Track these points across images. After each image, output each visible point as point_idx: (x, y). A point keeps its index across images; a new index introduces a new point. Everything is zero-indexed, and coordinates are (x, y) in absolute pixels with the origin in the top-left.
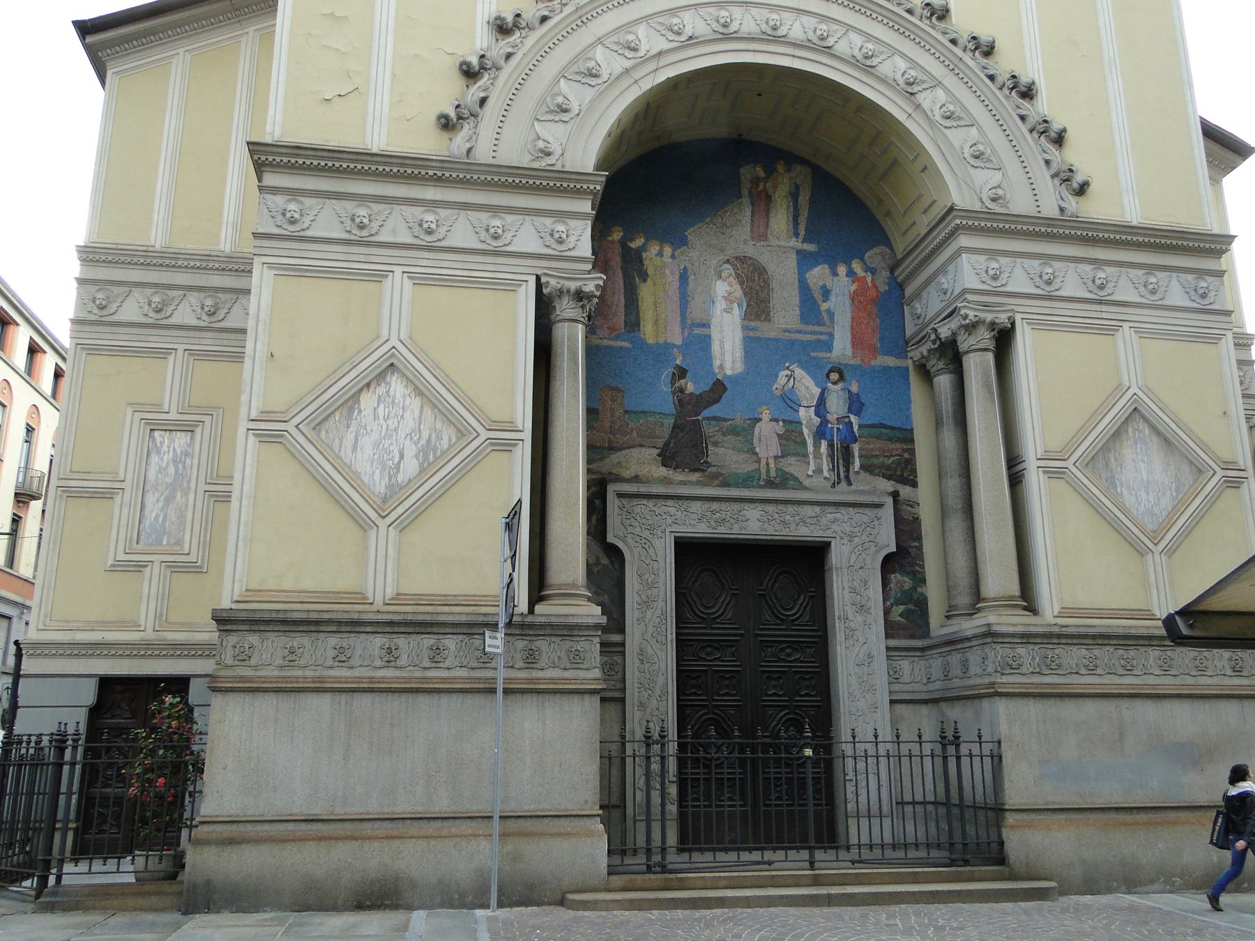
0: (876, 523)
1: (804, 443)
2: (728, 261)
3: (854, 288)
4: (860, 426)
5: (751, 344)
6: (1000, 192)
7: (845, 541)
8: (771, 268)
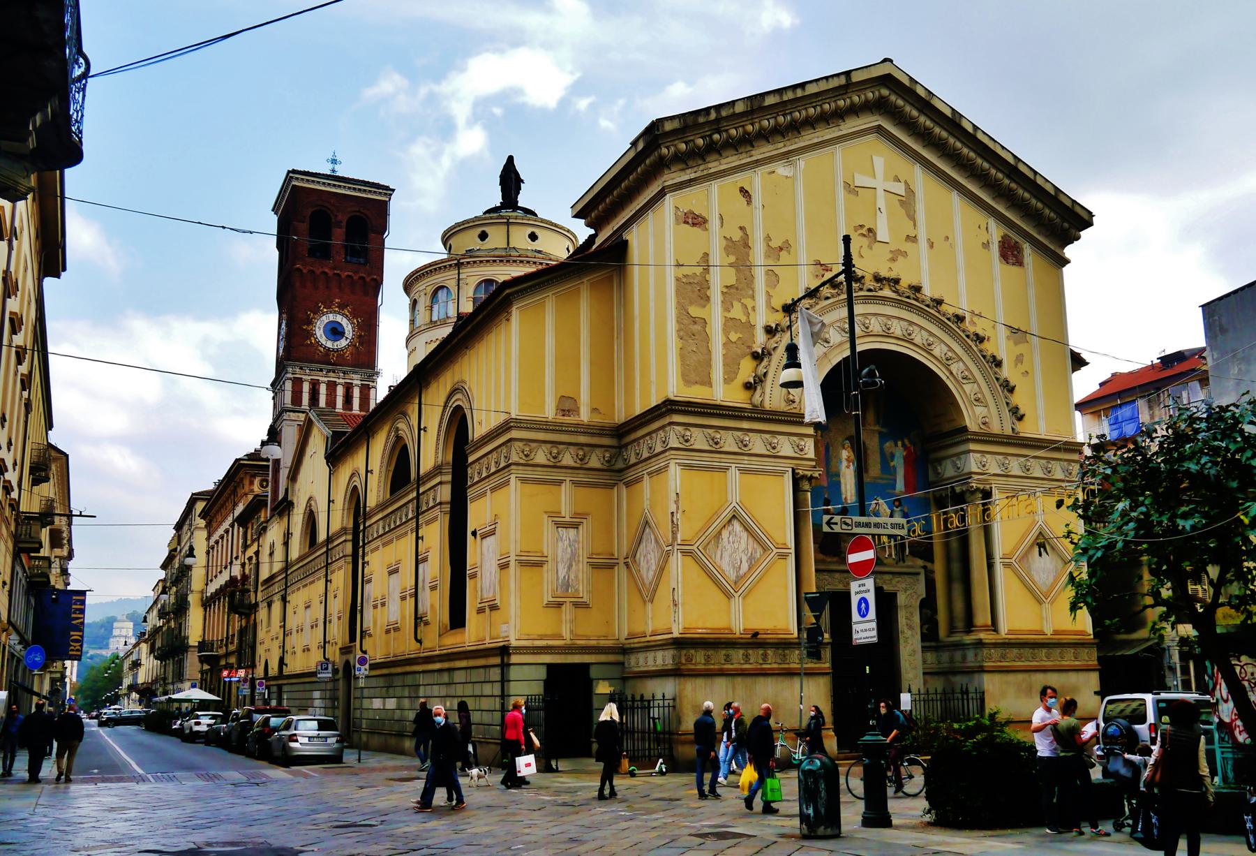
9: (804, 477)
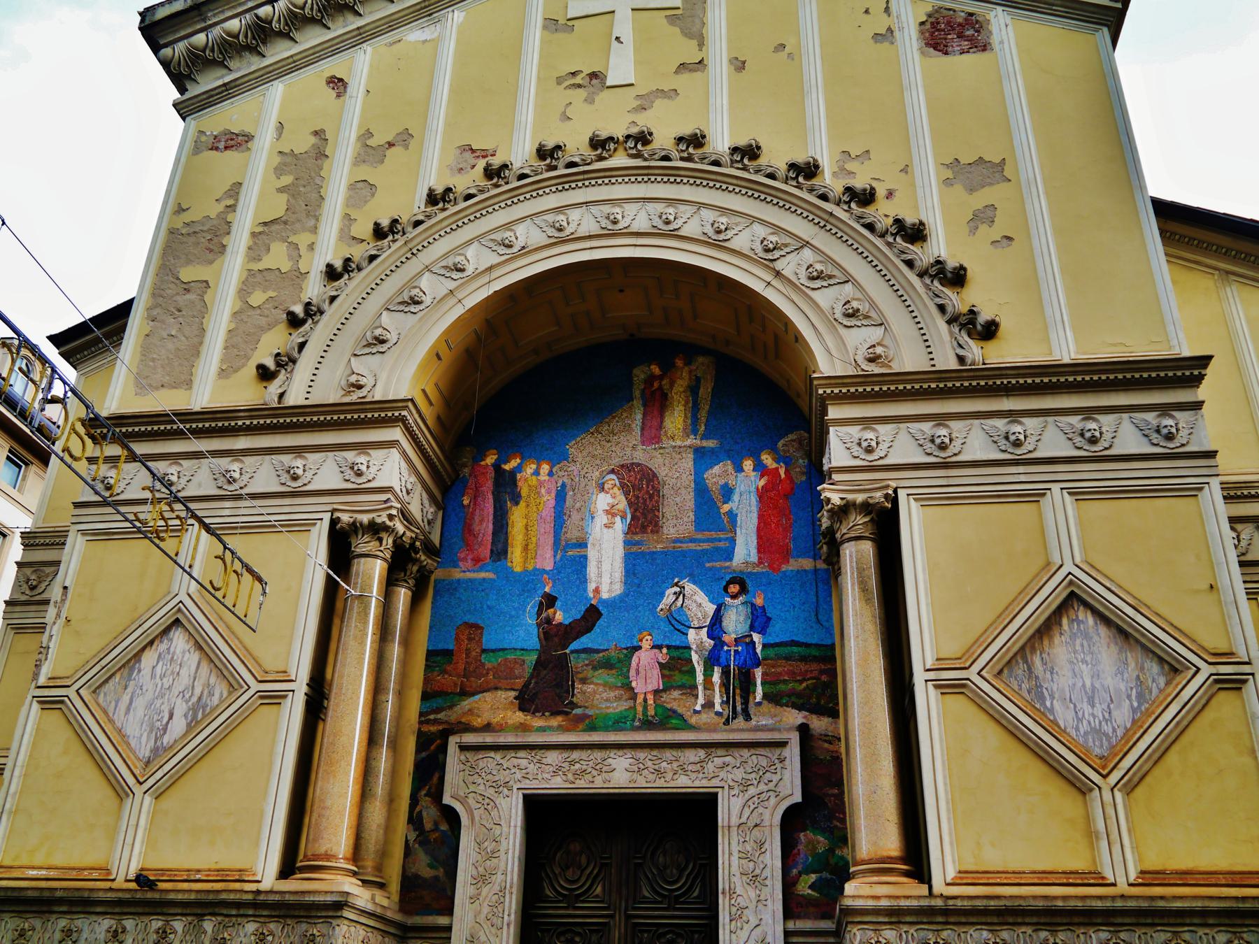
0: (778, 766)
1: (692, 672)
2: (613, 471)
3: (762, 483)
4: (764, 646)
5: (634, 562)
6: (879, 350)
7: (735, 792)
8: (662, 473)
9: (355, 528)
